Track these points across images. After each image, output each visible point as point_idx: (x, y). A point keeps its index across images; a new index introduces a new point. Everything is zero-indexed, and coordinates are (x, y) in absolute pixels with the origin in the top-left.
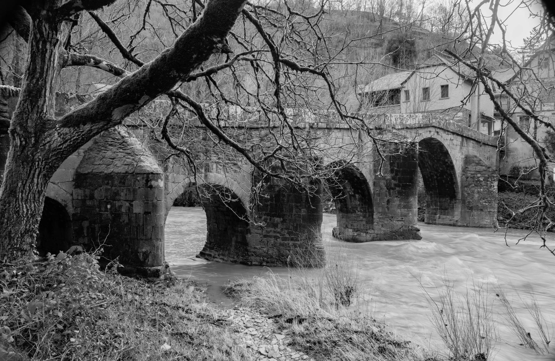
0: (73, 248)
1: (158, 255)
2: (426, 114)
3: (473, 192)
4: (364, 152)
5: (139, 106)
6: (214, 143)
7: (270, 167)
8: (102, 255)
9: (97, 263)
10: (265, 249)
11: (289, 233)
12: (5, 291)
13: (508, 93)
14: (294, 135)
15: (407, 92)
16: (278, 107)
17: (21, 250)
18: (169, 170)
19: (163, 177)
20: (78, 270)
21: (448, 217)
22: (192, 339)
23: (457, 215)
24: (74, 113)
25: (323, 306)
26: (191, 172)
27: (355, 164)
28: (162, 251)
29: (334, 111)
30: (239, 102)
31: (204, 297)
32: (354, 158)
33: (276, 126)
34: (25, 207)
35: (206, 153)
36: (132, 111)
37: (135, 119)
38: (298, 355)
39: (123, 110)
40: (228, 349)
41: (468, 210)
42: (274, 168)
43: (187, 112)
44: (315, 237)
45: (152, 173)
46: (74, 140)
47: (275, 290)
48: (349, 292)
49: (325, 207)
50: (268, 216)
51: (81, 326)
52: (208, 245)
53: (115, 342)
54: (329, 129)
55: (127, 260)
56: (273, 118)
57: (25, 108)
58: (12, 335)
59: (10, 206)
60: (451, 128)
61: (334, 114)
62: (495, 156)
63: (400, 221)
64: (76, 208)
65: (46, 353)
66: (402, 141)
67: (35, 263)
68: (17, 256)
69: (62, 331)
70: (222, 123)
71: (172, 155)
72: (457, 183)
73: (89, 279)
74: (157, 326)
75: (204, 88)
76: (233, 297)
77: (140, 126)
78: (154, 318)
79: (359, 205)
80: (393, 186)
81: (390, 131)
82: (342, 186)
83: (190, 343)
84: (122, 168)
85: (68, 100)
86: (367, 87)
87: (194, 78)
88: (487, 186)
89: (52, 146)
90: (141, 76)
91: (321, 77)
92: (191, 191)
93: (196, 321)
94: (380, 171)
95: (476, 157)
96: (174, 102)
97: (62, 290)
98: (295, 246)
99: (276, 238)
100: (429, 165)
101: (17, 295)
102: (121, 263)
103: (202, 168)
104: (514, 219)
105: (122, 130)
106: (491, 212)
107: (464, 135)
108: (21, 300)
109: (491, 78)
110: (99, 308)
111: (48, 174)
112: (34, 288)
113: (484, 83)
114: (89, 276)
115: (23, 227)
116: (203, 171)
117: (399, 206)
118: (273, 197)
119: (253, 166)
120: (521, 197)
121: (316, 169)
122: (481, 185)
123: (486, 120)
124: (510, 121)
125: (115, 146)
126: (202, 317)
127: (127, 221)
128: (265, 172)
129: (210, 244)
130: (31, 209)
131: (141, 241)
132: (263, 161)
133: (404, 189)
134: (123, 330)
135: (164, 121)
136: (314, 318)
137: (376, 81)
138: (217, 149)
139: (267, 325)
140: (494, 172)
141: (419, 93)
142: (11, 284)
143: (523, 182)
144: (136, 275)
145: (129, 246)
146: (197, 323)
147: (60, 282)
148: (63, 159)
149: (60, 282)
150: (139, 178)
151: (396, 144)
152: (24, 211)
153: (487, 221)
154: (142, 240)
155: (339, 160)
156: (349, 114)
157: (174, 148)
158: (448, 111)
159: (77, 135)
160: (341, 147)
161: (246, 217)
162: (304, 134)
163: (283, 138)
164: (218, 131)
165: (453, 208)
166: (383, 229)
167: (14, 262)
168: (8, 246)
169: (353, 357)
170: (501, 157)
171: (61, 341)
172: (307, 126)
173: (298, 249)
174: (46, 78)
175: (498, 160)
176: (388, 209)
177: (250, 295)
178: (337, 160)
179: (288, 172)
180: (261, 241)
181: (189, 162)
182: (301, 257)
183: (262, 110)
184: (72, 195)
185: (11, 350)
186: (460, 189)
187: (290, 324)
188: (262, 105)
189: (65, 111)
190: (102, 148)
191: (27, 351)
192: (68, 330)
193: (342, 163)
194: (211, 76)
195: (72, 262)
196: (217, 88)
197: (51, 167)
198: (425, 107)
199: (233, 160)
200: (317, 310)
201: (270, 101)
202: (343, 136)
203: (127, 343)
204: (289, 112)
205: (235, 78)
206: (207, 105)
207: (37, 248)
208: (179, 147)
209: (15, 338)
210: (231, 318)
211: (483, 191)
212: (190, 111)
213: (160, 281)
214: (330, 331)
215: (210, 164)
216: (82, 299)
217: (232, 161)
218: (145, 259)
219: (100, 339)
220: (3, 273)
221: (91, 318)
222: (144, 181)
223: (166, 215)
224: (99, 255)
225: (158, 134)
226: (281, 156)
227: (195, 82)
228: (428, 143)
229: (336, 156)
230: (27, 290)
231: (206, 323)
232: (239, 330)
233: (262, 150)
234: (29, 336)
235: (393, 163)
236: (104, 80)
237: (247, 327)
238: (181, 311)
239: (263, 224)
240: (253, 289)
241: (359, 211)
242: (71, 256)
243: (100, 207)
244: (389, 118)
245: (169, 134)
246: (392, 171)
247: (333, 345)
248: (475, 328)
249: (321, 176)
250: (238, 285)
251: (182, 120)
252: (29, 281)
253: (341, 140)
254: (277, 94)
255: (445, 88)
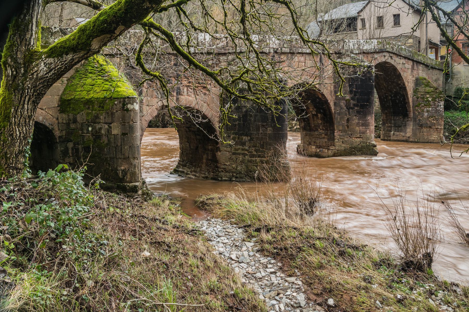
0: (60, 166)
1: (135, 172)
2: (380, 40)
3: (423, 111)
4: (325, 74)
5: (116, 35)
6: (185, 68)
7: (237, 89)
8: (86, 172)
9: (82, 180)
10: (234, 166)
11: (256, 151)
12: (4, 205)
13: (452, 21)
14: (260, 59)
15: (363, 20)
16: (244, 34)
17: (17, 169)
18: (143, 94)
19: (138, 101)
20: (66, 186)
21: (401, 133)
22: (170, 247)
23: (409, 131)
24: (57, 44)
25: (288, 215)
26: (164, 96)
27: (317, 86)
28: (139, 168)
29: (296, 37)
30: (207, 29)
31: (178, 210)
32: (315, 80)
33: (243, 51)
34: (17, 131)
35: (177, 77)
36: (109, 41)
37: (112, 48)
38: (266, 260)
39: (101, 40)
40: (203, 256)
41: (419, 127)
42: (241, 91)
43: (159, 41)
44: (280, 153)
45: (128, 97)
46: (58, 69)
47: (244, 203)
48: (312, 203)
49: (290, 126)
50: (236, 135)
51: (70, 235)
52: (181, 163)
53: (101, 249)
54: (293, 53)
55: (108, 177)
56: (239, 44)
57: (14, 42)
58: (13, 242)
59: (5, 129)
60: (403, 53)
61: (296, 39)
62: (441, 79)
63: (359, 138)
64: (62, 131)
65: (42, 258)
66: (360, 64)
67: (29, 180)
68: (13, 174)
69: (55, 239)
70: (192, 50)
71: (146, 80)
72: (409, 103)
73: (75, 193)
74: (137, 236)
75: (175, 18)
76: (206, 209)
77: (117, 54)
78: (134, 228)
79: (321, 123)
80: (352, 106)
81: (348, 56)
82: (305, 106)
83: (167, 250)
84: (101, 93)
85: (52, 34)
86: (327, 15)
87: (165, 9)
88: (435, 105)
89: (39, 75)
90: (117, 8)
91: (284, 6)
92: (164, 114)
93: (172, 231)
94: (340, 92)
95: (425, 79)
96: (147, 31)
97: (53, 204)
98: (262, 162)
99: (244, 155)
100: (384, 86)
101: (15, 208)
102: (102, 179)
103: (174, 92)
104: (458, 135)
105: (100, 59)
106: (438, 128)
107: (415, 59)
108: (19, 212)
109: (437, 8)
110: (85, 219)
111: (36, 100)
112: (28, 202)
113: (431, 11)
114: (75, 191)
115: (17, 149)
116: (175, 94)
117: (358, 124)
118: (240, 117)
119: (221, 88)
120: (463, 115)
121: (281, 91)
122: (430, 104)
123: (433, 46)
124: (455, 47)
125: (95, 73)
126: (178, 228)
127: (106, 142)
128: (233, 93)
129: (183, 162)
130: (23, 132)
131: (120, 160)
132: (231, 84)
133: (363, 109)
134: (108, 239)
135: (138, 49)
136: (281, 227)
137: (335, 10)
138: (188, 73)
139: (237, 234)
140: (440, 93)
141: (374, 21)
142: (10, 199)
143: (465, 102)
144: (116, 191)
145: (109, 164)
146: (173, 233)
147: (50, 197)
148: (49, 86)
149: (50, 197)
150: (116, 102)
151: (354, 66)
152: (17, 134)
153: (434, 137)
154: (121, 158)
155: (302, 82)
156: (311, 40)
157: (148, 73)
158: (400, 37)
159: (60, 64)
160: (304, 70)
161: (216, 136)
162: (269, 58)
163: (250, 62)
164: (188, 57)
165: (406, 125)
166: (343, 145)
167: (10, 179)
168: (5, 165)
169: (316, 260)
170: (447, 80)
171: (55, 248)
172: (272, 51)
173: (265, 165)
174: (32, 13)
175: (444, 83)
176: (348, 127)
177: (221, 207)
178: (300, 82)
179: (254, 93)
180: (230, 159)
181: (161, 87)
182: (268, 172)
183: (229, 37)
184: (57, 119)
185: (12, 256)
186: (411, 108)
187: (259, 233)
188: (229, 32)
189: (50, 44)
190: (83, 76)
191: (27, 256)
192: (60, 239)
193: (305, 85)
194: (182, 6)
195: (60, 179)
196: (187, 17)
197: (38, 94)
198: (380, 34)
199: (202, 83)
200: (284, 220)
201: (236, 28)
202: (306, 60)
203: (112, 250)
204: (254, 38)
205: (204, 8)
206: (177, 33)
207: (30, 167)
208: (152, 73)
209: (16, 245)
210: (204, 228)
211: (432, 110)
212: (162, 39)
213: (138, 195)
214: (295, 238)
215: (181, 88)
216: (70, 211)
217: (202, 85)
218: (124, 177)
219: (88, 246)
220: (2, 189)
221: (79, 229)
222: (121, 105)
223: (142, 136)
224: (83, 173)
225: (133, 61)
226: (248, 79)
227: (167, 13)
228: (382, 66)
229: (299, 78)
230: (23, 204)
231: (182, 233)
232: (212, 239)
233: (230, 73)
234: (27, 243)
235: (352, 85)
236: (84, 15)
237: (219, 237)
238: (158, 222)
239: (232, 142)
240: (224, 202)
241: (321, 130)
242: (58, 174)
243: (82, 130)
244: (348, 44)
245: (143, 61)
246: (351, 92)
247: (298, 250)
248: (423, 231)
249: (286, 97)
250: (210, 199)
251: (155, 48)
252: (24, 196)
253: (304, 63)
254: (243, 21)
255: (397, 17)
